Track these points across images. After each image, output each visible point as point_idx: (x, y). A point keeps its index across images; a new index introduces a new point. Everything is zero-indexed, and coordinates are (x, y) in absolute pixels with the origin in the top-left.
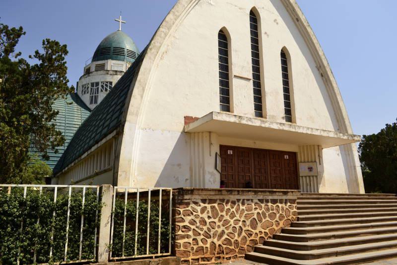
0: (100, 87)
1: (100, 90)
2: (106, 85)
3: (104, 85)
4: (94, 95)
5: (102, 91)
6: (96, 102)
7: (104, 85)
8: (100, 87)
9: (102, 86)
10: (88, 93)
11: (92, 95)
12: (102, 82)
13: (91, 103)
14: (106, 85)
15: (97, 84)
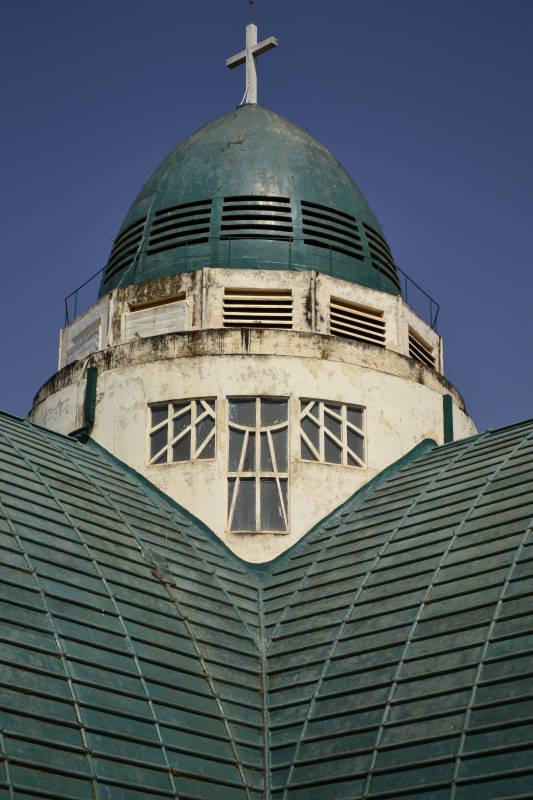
1: (294, 447)
2: (333, 423)
3: (321, 421)
4: (258, 474)
5: (307, 454)
6: (276, 522)
7: (321, 421)
9: (308, 424)
10: (209, 453)
11: (240, 473)
12: (304, 402)
13: (242, 521)
14: (333, 423)
15: (275, 404)
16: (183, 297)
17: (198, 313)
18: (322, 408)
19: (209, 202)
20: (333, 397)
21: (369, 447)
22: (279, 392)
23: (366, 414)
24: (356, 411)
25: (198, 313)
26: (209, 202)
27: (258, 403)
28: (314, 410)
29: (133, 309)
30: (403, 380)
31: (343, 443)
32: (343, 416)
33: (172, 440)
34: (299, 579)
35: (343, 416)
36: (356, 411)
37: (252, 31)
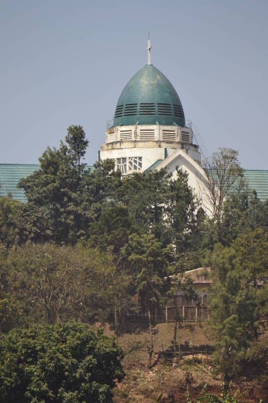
0: (128, 164)
2: (135, 161)
3: (133, 161)
7: (133, 161)
8: (128, 164)
9: (130, 163)
12: (130, 158)
14: (135, 161)
15: (124, 159)
16: (114, 132)
17: (116, 137)
18: (133, 159)
19: (137, 104)
20: (135, 156)
21: (143, 165)
22: (124, 157)
23: (143, 159)
24: (140, 158)
25: (116, 137)
26: (137, 104)
27: (121, 160)
28: (132, 160)
29: (110, 133)
30: (152, 149)
31: (137, 165)
32: (137, 160)
33: (134, 163)
34: (4, 193)
35: (137, 160)
36: (140, 158)
37: (149, 42)
